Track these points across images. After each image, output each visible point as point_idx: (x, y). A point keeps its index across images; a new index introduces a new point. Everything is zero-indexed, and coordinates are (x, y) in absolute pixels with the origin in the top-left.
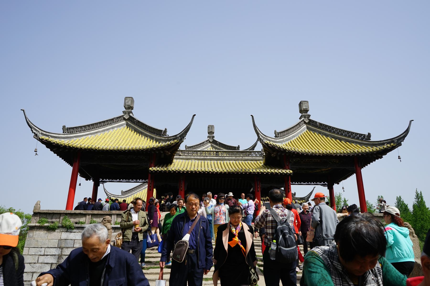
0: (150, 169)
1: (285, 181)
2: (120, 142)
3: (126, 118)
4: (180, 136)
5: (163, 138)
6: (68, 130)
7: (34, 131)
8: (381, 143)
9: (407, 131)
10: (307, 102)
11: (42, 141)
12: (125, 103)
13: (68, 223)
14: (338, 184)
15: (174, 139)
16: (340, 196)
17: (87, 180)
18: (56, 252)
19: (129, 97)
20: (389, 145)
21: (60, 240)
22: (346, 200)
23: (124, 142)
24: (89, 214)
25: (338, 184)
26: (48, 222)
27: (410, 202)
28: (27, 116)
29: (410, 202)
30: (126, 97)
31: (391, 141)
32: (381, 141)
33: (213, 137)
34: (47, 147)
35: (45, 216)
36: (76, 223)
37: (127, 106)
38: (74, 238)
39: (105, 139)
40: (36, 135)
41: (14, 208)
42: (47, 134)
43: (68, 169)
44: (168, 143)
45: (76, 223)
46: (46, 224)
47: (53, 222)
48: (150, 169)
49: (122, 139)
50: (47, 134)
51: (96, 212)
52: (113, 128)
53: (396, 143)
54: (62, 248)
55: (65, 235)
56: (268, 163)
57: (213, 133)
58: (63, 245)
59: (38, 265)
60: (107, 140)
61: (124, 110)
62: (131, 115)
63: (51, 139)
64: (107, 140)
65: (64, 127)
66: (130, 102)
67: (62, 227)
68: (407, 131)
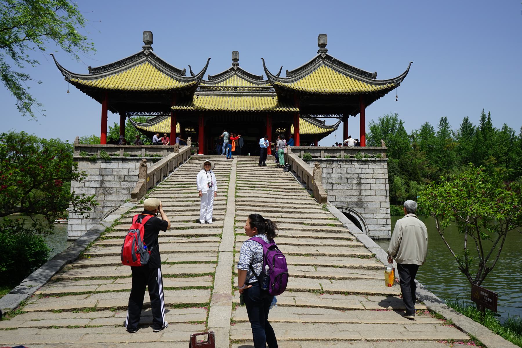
0: (151, 309)
1: (294, 119)
2: (143, 81)
3: (147, 54)
4: (197, 78)
5: (183, 79)
6: (96, 71)
7: (65, 74)
8: (383, 83)
9: (407, 72)
10: (326, 35)
11: (73, 83)
12: (144, 38)
13: (105, 156)
14: (355, 116)
15: (192, 81)
16: (396, 117)
17: (113, 113)
18: (99, 178)
19: (148, 32)
20: (389, 85)
21: (100, 169)
22: (402, 122)
23: (146, 81)
24: (122, 148)
25: (355, 116)
26: (88, 155)
27: (476, 123)
28: (57, 60)
29: (476, 123)
30: (145, 32)
31: (392, 81)
32: (384, 81)
33: (238, 65)
34: (77, 88)
35: (85, 150)
36: (112, 155)
37: (146, 42)
38: (112, 168)
39: (128, 77)
40: (67, 78)
41: (26, 132)
42: (77, 76)
43: (99, 106)
44: (187, 84)
45: (112, 155)
46: (87, 156)
47: (92, 155)
48: (172, 108)
49: (144, 78)
50: (77, 76)
51: (127, 146)
52: (134, 65)
53: (396, 83)
54: (103, 176)
55: (104, 165)
56: (282, 102)
57: (238, 60)
58: (103, 173)
59: (85, 188)
60: (131, 79)
61: (144, 45)
62: (151, 50)
63: (80, 81)
64: (131, 79)
65: (90, 68)
66: (149, 37)
67: (101, 159)
68: (407, 72)
